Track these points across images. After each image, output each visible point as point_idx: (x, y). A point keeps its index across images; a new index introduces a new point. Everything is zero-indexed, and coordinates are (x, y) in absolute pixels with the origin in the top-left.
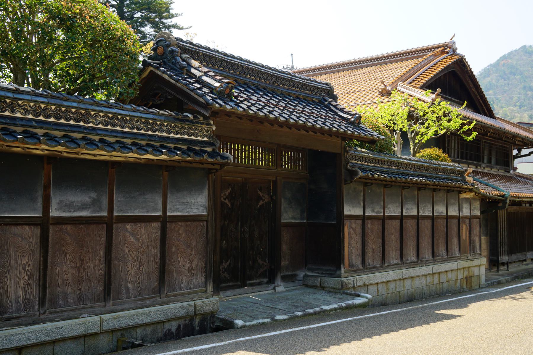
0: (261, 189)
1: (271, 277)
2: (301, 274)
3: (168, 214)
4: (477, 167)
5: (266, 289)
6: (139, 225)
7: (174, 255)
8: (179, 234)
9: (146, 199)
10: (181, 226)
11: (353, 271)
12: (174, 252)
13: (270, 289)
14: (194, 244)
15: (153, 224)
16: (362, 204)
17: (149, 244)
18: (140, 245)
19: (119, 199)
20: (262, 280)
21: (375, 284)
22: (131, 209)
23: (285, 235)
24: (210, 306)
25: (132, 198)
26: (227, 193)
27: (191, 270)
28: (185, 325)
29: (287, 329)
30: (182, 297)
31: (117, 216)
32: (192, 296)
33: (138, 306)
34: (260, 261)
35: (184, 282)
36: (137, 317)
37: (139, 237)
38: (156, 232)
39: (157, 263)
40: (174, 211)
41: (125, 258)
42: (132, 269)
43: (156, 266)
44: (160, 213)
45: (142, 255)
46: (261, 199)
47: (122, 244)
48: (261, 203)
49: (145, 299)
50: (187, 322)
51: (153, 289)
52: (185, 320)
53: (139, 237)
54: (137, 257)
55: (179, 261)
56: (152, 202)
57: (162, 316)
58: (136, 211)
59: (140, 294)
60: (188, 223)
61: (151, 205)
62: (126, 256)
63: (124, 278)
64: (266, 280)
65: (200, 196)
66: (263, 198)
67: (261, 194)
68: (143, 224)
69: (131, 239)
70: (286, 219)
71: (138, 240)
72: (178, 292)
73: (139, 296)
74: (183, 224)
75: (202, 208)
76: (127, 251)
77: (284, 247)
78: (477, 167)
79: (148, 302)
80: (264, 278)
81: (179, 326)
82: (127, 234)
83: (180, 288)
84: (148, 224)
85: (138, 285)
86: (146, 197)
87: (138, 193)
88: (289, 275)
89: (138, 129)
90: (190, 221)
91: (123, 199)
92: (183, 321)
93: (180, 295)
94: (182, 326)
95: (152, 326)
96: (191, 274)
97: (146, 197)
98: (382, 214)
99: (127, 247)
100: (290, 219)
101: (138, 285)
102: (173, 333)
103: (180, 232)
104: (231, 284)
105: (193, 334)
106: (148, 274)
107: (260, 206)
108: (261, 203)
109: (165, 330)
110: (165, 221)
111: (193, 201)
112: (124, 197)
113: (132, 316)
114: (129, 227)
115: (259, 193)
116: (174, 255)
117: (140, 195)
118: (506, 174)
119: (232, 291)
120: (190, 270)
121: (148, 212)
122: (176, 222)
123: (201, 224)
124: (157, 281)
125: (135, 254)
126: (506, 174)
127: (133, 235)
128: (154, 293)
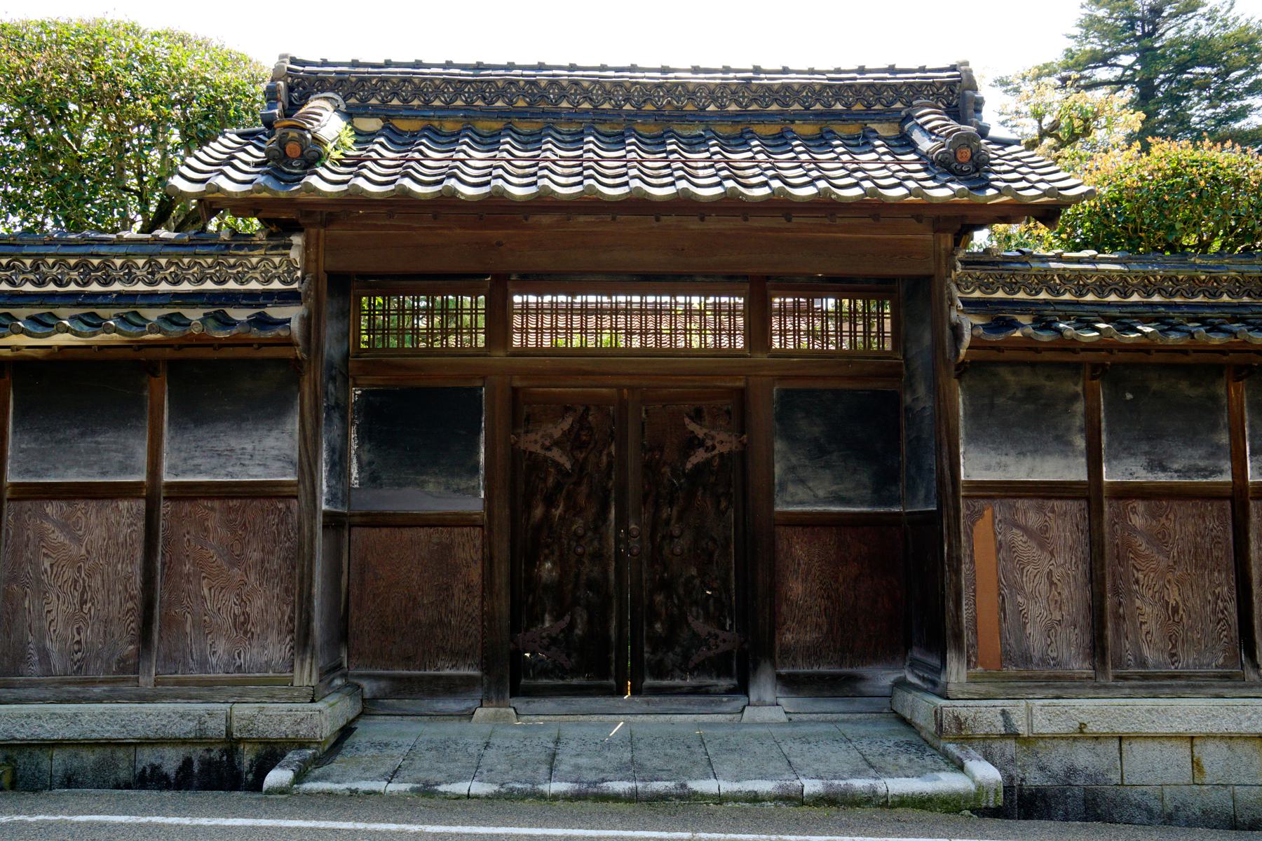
0: (697, 416)
1: (735, 671)
2: (884, 677)
3: (777, 509)
4: (702, 219)
5: (703, 709)
6: (81, 504)
7: (189, 582)
8: (206, 530)
9: (96, 442)
10: (212, 509)
11: (1024, 678)
12: (188, 575)
13: (729, 709)
14: (256, 556)
15: (123, 505)
16: (1080, 442)
17: (111, 551)
18: (83, 551)
19: (23, 446)
20: (709, 681)
21: (1178, 737)
22: (56, 468)
23: (799, 552)
24: (281, 722)
25: (59, 442)
26: (557, 434)
27: (243, 624)
28: (207, 764)
29: (479, 824)
30: (208, 688)
31: (14, 485)
32: (239, 689)
33: (65, 695)
34: (700, 626)
35: (220, 651)
36: (38, 722)
37: (81, 533)
38: (132, 524)
39: (132, 598)
40: (184, 472)
41: (40, 581)
42: (59, 607)
43: (130, 605)
44: (141, 477)
45: (89, 576)
46: (701, 443)
47: (31, 547)
48: (699, 456)
49: (93, 682)
50: (215, 754)
51: (119, 662)
52: (209, 750)
53: (81, 533)
54: (76, 581)
55: (204, 597)
56: (116, 451)
57: (116, 728)
58: (70, 472)
59: (80, 668)
60: (234, 503)
61: (120, 457)
62: (44, 577)
63: (36, 625)
64: (724, 683)
65: (275, 433)
66: (709, 443)
67: (700, 432)
68: (93, 503)
69: (58, 537)
70: (801, 503)
71: (79, 540)
72: (197, 675)
73: (75, 673)
74: (217, 504)
75: (279, 464)
76: (47, 564)
77: (796, 588)
78: (702, 219)
79: (97, 690)
80: (718, 677)
81: (188, 762)
82: (47, 525)
83: (203, 664)
84: (106, 502)
85: (76, 647)
86: (99, 439)
87: (76, 431)
88: (821, 677)
89: (59, 283)
90: (241, 498)
91: (33, 445)
92: (200, 751)
93: (200, 683)
94: (196, 764)
95: (98, 750)
96: (246, 633)
97: (99, 439)
98: (1227, 478)
99: (45, 555)
100: (818, 501)
101: (76, 647)
102: (166, 777)
103: (209, 524)
104: (575, 682)
105: (235, 788)
106: (107, 622)
107: (696, 466)
108: (699, 456)
109: (140, 767)
110: (151, 494)
111: (249, 447)
112: (36, 440)
113: (21, 716)
114: (51, 508)
115: (692, 426)
116: (189, 582)
117: (83, 435)
118: (788, 225)
119: (560, 700)
120: (242, 625)
121: (104, 474)
122: (195, 498)
123: (280, 506)
124: (131, 643)
125: (69, 574)
126: (788, 225)
127: (64, 527)
128: (122, 670)
